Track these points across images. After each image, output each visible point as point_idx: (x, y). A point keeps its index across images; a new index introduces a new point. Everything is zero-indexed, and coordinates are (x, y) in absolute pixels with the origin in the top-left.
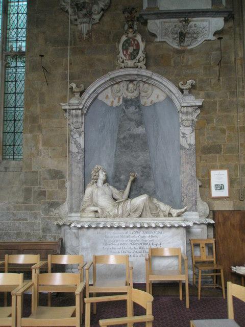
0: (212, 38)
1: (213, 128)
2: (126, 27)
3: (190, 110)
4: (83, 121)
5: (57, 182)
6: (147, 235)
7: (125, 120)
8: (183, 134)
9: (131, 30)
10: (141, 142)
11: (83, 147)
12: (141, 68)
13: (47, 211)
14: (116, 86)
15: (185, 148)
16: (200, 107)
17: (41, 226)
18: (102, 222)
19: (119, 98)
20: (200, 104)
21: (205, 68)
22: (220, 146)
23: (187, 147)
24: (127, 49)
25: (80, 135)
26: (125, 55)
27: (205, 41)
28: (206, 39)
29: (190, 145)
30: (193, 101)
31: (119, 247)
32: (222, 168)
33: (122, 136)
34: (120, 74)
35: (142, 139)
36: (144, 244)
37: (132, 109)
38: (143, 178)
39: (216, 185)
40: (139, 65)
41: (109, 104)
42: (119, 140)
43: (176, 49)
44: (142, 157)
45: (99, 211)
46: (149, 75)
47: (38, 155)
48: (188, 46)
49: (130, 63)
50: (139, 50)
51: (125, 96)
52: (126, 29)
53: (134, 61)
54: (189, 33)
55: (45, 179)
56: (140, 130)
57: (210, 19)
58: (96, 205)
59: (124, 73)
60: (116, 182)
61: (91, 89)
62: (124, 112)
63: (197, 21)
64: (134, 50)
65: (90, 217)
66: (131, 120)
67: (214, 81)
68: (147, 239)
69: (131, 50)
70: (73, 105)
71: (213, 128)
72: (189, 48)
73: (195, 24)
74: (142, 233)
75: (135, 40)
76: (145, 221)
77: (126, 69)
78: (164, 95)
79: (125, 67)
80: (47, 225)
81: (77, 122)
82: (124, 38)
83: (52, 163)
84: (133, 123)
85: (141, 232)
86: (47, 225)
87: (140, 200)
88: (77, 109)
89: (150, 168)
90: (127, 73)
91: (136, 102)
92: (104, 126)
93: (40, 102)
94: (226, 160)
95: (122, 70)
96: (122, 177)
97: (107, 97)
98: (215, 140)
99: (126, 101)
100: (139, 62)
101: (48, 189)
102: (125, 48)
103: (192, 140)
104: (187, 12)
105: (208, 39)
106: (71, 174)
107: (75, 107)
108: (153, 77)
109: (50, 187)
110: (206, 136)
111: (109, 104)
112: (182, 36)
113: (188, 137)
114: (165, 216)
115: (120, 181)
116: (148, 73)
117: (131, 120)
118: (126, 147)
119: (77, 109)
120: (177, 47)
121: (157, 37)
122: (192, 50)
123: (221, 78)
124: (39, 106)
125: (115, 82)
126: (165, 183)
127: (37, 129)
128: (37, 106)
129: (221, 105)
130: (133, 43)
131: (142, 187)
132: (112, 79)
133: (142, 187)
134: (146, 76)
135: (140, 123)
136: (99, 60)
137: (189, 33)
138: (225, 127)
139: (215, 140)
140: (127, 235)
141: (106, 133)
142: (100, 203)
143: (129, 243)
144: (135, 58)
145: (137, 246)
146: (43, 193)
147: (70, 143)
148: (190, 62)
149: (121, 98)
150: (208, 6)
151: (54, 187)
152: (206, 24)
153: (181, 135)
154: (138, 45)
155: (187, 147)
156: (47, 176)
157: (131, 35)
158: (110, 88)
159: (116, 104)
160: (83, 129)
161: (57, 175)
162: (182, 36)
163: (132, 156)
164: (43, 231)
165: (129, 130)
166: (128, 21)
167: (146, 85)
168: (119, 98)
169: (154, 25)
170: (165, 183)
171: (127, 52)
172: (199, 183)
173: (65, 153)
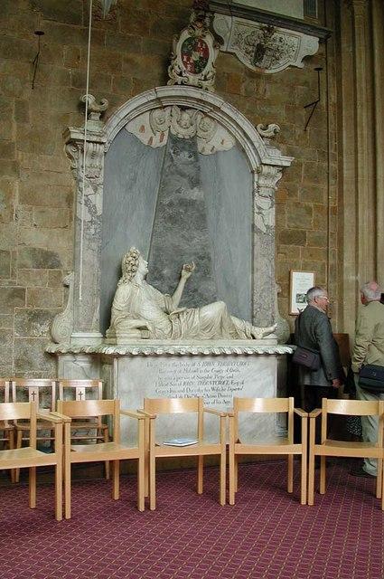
0: (299, 64)
1: (297, 205)
2: (193, 17)
3: (273, 171)
4: (103, 165)
5: (46, 273)
6: (224, 368)
7: (172, 173)
8: (259, 208)
9: (199, 25)
10: (197, 214)
11: (100, 212)
12: (207, 89)
13: (25, 327)
14: (157, 113)
15: (261, 232)
16: (283, 169)
17: (13, 355)
18: (148, 346)
19: (163, 135)
20: (288, 164)
21: (288, 109)
22: (304, 233)
23: (264, 230)
24: (189, 55)
25: (96, 190)
26: (185, 64)
27: (290, 66)
28: (292, 64)
29: (267, 227)
30: (279, 158)
31: (182, 388)
32: (305, 269)
33: (166, 201)
34: (174, 93)
35: (198, 210)
36: (220, 382)
37: (184, 156)
38: (198, 275)
39: (299, 295)
40: (205, 84)
41: (146, 142)
42: (160, 205)
43: (249, 70)
44: (198, 239)
45: (150, 328)
46: (217, 104)
47: (11, 219)
48: (266, 68)
49: (193, 79)
50: (207, 60)
51: (174, 132)
52: (192, 21)
53: (199, 76)
54: (270, 50)
55: (24, 266)
56: (195, 194)
57: (301, 34)
58: (138, 316)
59: (179, 93)
60: (156, 279)
61: (124, 111)
62: (172, 160)
63: (284, 33)
64: (200, 58)
65: (134, 337)
66: (183, 175)
67: (299, 131)
68: (224, 374)
69: (195, 57)
70: (90, 133)
71: (297, 205)
72: (267, 72)
73: (281, 38)
74: (216, 365)
75: (203, 42)
76: (228, 345)
77: (185, 88)
78: (234, 141)
79: (182, 84)
80: (25, 354)
81: (91, 166)
82: (185, 35)
83: (38, 238)
84: (185, 180)
85: (216, 363)
86: (25, 354)
87: (212, 311)
88: (96, 143)
89: (209, 260)
90: (184, 94)
91: (190, 144)
92: (135, 180)
93: (17, 119)
94: (311, 255)
95: (177, 87)
96: (165, 272)
97: (143, 129)
98: (298, 223)
99: (174, 140)
100: (205, 79)
101: (29, 286)
102: (186, 54)
103: (271, 221)
104: (273, 17)
105: (294, 64)
106: (74, 261)
107: (95, 139)
108: (223, 109)
109: (35, 281)
110: (287, 215)
111: (146, 142)
112: (260, 52)
113: (267, 217)
114: (248, 338)
115: (161, 277)
116: (217, 101)
117: (183, 175)
118: (173, 219)
119: (96, 143)
120: (251, 67)
121: (223, 44)
122: (270, 76)
123: (308, 128)
124: (15, 125)
125: (160, 104)
126: (228, 286)
127: (10, 168)
128: (11, 127)
129: (307, 171)
130: (199, 46)
131: (196, 290)
132: (158, 99)
133: (196, 290)
134: (211, 105)
135: (195, 183)
136: (128, 61)
137: (270, 50)
138: (312, 205)
139: (298, 223)
140: (193, 368)
141: (138, 192)
142: (145, 314)
143: (196, 381)
144: (200, 71)
145: (209, 387)
146: (18, 294)
147: (78, 204)
148: (268, 95)
149: (166, 133)
150: (298, 14)
151: (40, 283)
152: (295, 40)
153: (256, 210)
154: (206, 51)
155: (264, 230)
156: (29, 262)
157: (198, 32)
158: (148, 113)
159: (156, 143)
160: (101, 180)
161: (47, 260)
162: (260, 52)
163: (183, 236)
164: (18, 366)
165: (178, 191)
166: (198, 9)
167: (207, 120)
168: (163, 135)
169: (224, 23)
170: (228, 286)
171: (188, 59)
172: (277, 289)
173: (69, 221)
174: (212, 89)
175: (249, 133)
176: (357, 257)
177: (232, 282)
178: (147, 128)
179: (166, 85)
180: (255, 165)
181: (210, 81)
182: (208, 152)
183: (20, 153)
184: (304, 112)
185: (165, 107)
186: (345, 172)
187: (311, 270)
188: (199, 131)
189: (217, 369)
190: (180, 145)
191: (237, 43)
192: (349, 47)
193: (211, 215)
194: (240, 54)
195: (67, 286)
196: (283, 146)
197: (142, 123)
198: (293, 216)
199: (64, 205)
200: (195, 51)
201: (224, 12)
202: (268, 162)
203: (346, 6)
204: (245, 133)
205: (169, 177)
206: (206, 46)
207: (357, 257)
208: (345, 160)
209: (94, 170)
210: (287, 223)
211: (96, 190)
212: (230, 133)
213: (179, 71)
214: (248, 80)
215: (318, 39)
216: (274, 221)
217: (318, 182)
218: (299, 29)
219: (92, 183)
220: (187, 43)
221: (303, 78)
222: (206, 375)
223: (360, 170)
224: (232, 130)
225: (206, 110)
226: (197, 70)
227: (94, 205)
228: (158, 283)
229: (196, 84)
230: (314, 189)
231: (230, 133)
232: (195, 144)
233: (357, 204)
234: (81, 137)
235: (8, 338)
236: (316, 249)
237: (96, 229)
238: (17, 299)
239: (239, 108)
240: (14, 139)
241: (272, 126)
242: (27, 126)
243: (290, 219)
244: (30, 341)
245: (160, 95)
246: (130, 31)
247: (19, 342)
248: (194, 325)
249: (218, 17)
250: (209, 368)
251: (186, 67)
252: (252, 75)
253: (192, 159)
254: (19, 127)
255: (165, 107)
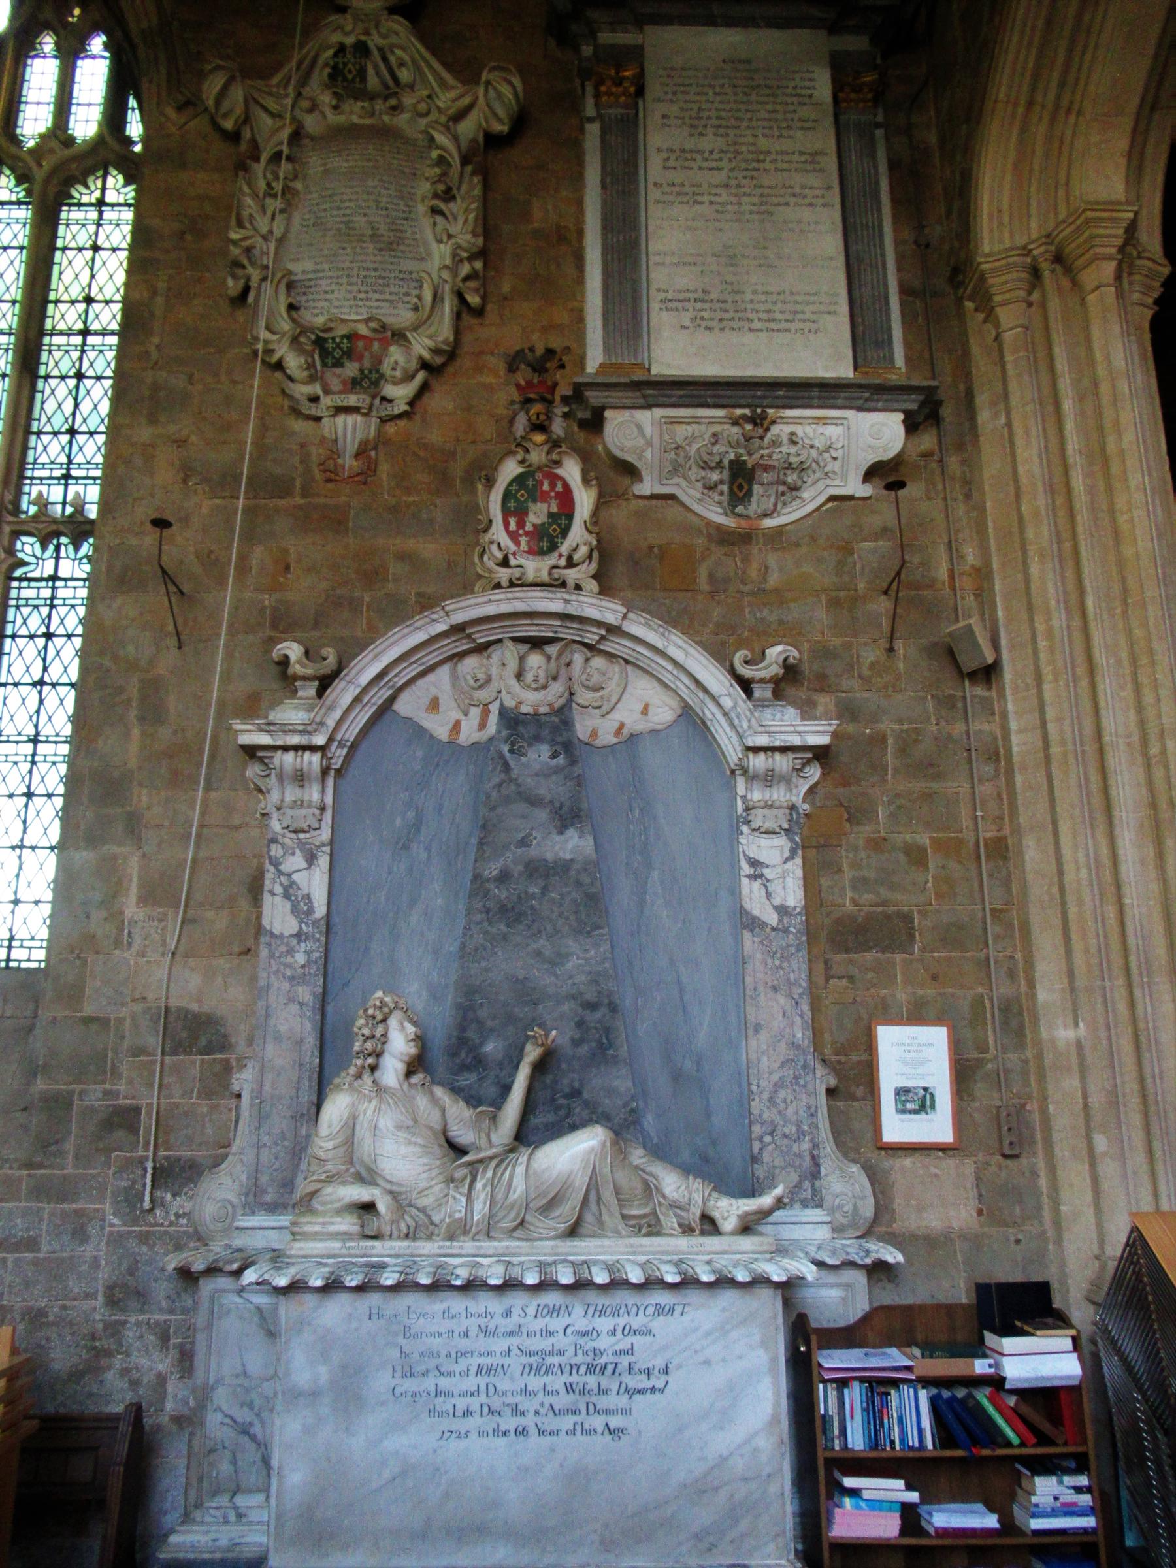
1: (877, 844)
3: (782, 763)
4: (329, 800)
5: (194, 1065)
6: (604, 1324)
7: (507, 800)
8: (754, 863)
9: (539, 438)
10: (575, 895)
11: (320, 911)
12: (578, 587)
14: (471, 662)
15: (763, 925)
16: (820, 754)
19: (486, 712)
20: (824, 740)
21: (834, 603)
22: (907, 919)
23: (772, 919)
24: (521, 514)
25: (311, 859)
26: (514, 536)
27: (832, 498)
29: (782, 910)
31: (471, 1383)
32: (916, 1016)
33: (492, 869)
34: (491, 610)
35: (579, 884)
36: (591, 1369)
37: (540, 755)
38: (584, 1049)
40: (572, 575)
43: (719, 527)
45: (382, 1207)
46: (611, 619)
48: (766, 515)
49: (535, 568)
53: (552, 560)
54: (767, 468)
59: (505, 608)
60: (464, 1067)
62: (506, 768)
63: (798, 421)
64: (551, 515)
65: (336, 1236)
66: (534, 801)
67: (871, 655)
68: (604, 1342)
69: (537, 514)
70: (286, 729)
71: (877, 844)
72: (769, 523)
73: (793, 434)
75: (553, 478)
77: (518, 593)
78: (674, 703)
79: (512, 584)
81: (300, 804)
86: (131, 1272)
89: (613, 1008)
90: (520, 606)
92: (417, 825)
93: (142, 719)
94: (934, 978)
95: (498, 595)
97: (434, 704)
99: (512, 720)
100: (571, 564)
101: (149, 1100)
102: (514, 509)
103: (792, 893)
107: (295, 740)
110: (848, 874)
111: (442, 732)
114: (687, 1230)
116: (609, 611)
117: (534, 801)
120: (720, 519)
121: (641, 480)
122: (780, 531)
123: (899, 645)
128: (127, 735)
130: (546, 487)
132: (458, 629)
133: (576, 1093)
134: (599, 624)
136: (402, 557)
137: (767, 468)
138: (924, 839)
140: (510, 1323)
143: (515, 1363)
144: (554, 547)
147: (266, 896)
148: (773, 580)
149: (495, 708)
152: (832, 431)
153: (746, 869)
154: (566, 499)
155: (772, 919)
158: (444, 672)
159: (469, 733)
164: (113, 1302)
165: (524, 843)
167: (598, 662)
168: (486, 712)
170: (677, 1077)
171: (521, 524)
174: (593, 586)
175: (703, 676)
176: (1071, 974)
177: (688, 1065)
178: (446, 701)
179: (472, 592)
180: (732, 752)
181: (584, 567)
182: (607, 737)
183: (145, 791)
184: (883, 605)
185: (488, 645)
186: (1015, 739)
187: (937, 1022)
188: (577, 688)
189: (582, 1324)
190: (530, 730)
191: (676, 469)
192: (996, 415)
193: (622, 897)
194: (690, 494)
195: (239, 1096)
196: (825, 701)
197: (434, 691)
198: (871, 874)
199: (244, 904)
200: (535, 501)
201: (628, 402)
202: (762, 741)
203: (981, 316)
204: (697, 682)
205: (499, 810)
206: (566, 486)
207: (1071, 974)
208: (1010, 707)
209: (304, 812)
210: (849, 894)
211: (311, 859)
212: (666, 686)
213: (499, 555)
214: (718, 552)
215: (901, 416)
216: (800, 894)
217: (939, 776)
218: (840, 402)
219: (301, 844)
220: (514, 487)
221: (875, 521)
222: (544, 1344)
223: (1051, 727)
224: (667, 678)
225: (591, 638)
226: (545, 544)
227: (308, 896)
228: (468, 1079)
229: (545, 577)
230: (928, 796)
231: (666, 686)
232: (567, 724)
233: (1055, 823)
234: (265, 739)
235: (92, 1230)
236: (949, 959)
237: (308, 953)
238: (120, 1134)
239: (678, 620)
240: (133, 763)
241: (775, 652)
242: (165, 733)
243: (860, 884)
244: (144, 1238)
245: (459, 618)
246: (408, 491)
247: (117, 1240)
248: (513, 1197)
249: (614, 420)
250: (556, 1324)
251: (518, 544)
252: (725, 538)
253: (561, 760)
254: (143, 733)
255: (488, 645)
